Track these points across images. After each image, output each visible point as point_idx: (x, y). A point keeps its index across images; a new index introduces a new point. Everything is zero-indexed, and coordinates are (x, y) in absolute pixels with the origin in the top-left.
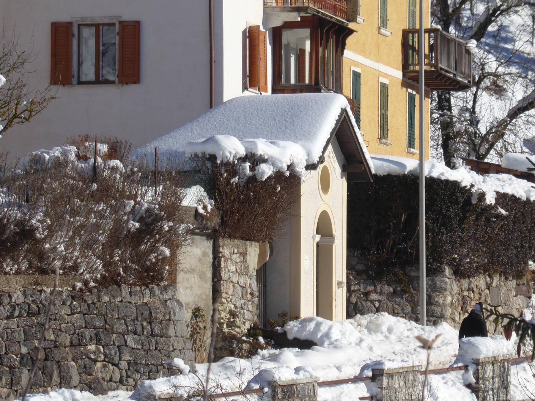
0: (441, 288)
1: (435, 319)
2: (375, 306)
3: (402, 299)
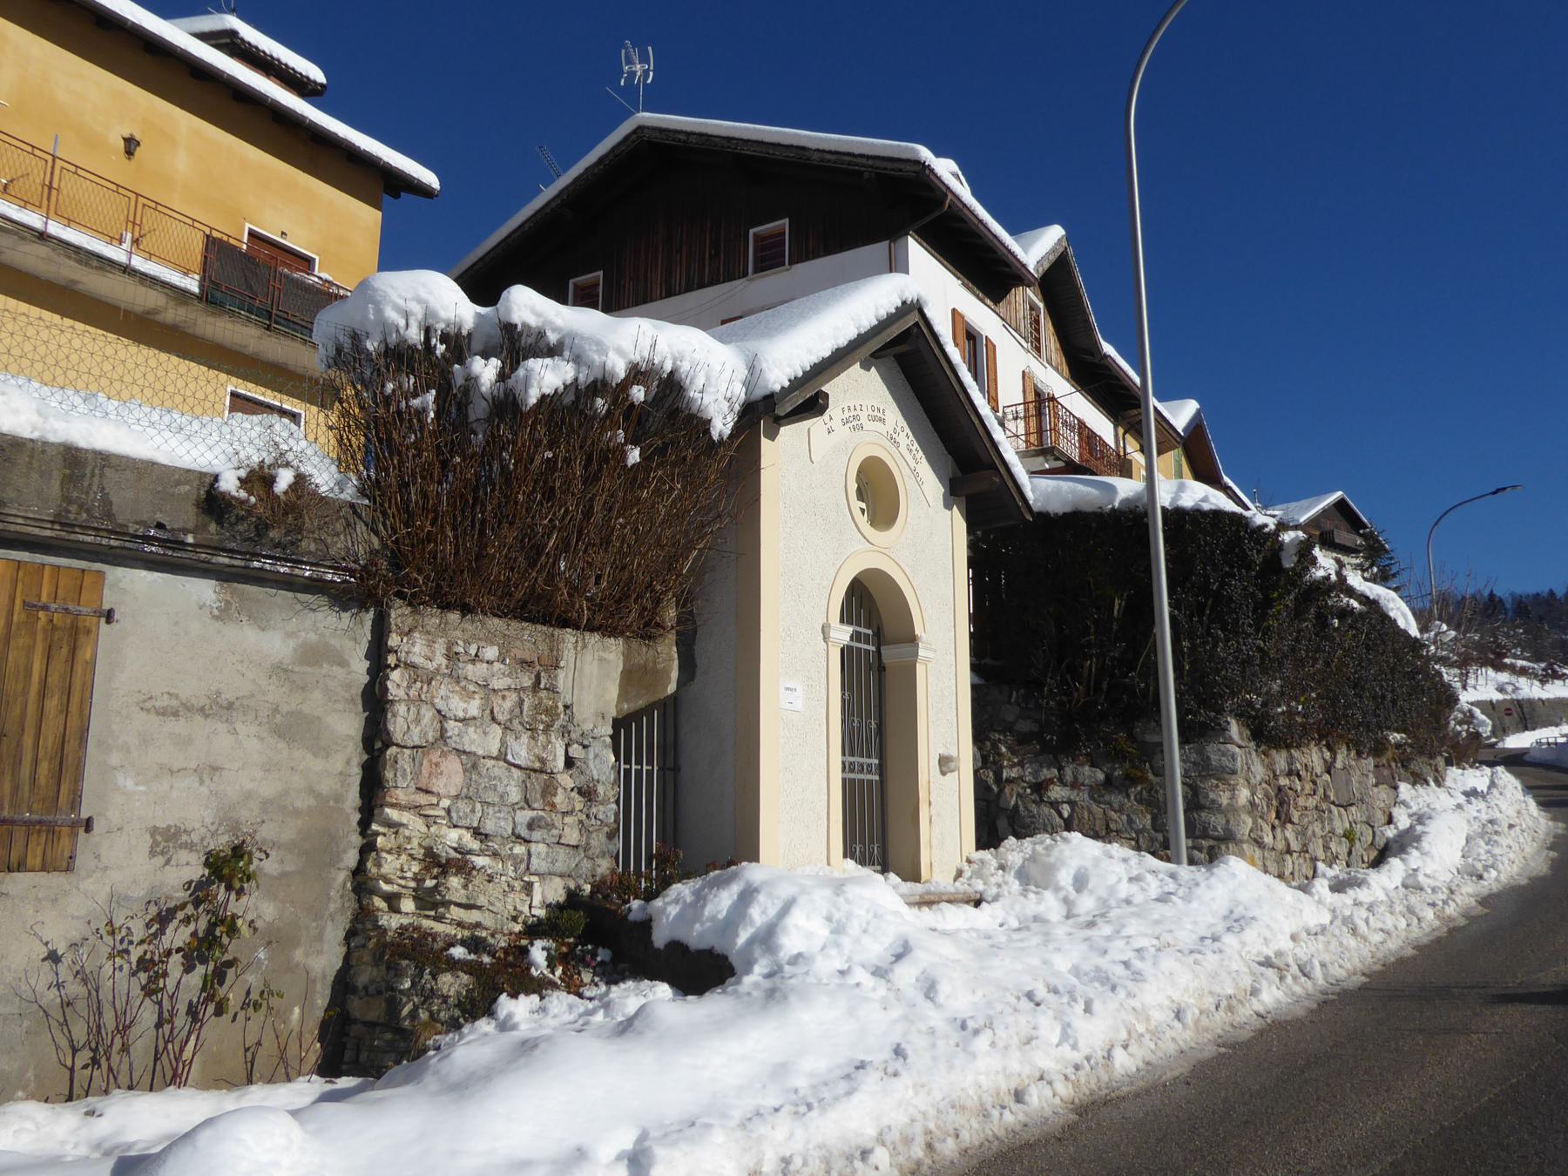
0: (1223, 769)
1: (1212, 842)
2: (1061, 815)
3: (1128, 796)
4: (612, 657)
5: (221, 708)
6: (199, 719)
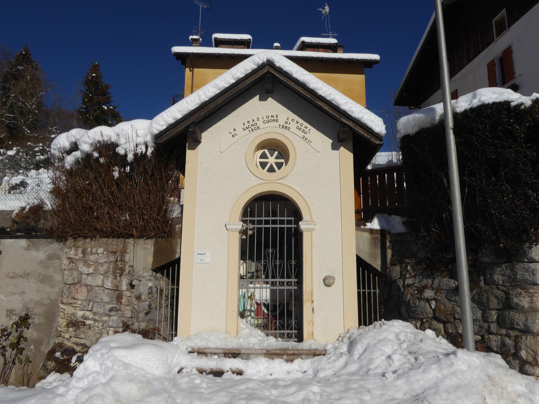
0: (526, 281)
1: (517, 333)
4: (149, 246)
5: (26, 275)
6: (20, 278)
